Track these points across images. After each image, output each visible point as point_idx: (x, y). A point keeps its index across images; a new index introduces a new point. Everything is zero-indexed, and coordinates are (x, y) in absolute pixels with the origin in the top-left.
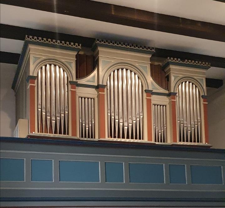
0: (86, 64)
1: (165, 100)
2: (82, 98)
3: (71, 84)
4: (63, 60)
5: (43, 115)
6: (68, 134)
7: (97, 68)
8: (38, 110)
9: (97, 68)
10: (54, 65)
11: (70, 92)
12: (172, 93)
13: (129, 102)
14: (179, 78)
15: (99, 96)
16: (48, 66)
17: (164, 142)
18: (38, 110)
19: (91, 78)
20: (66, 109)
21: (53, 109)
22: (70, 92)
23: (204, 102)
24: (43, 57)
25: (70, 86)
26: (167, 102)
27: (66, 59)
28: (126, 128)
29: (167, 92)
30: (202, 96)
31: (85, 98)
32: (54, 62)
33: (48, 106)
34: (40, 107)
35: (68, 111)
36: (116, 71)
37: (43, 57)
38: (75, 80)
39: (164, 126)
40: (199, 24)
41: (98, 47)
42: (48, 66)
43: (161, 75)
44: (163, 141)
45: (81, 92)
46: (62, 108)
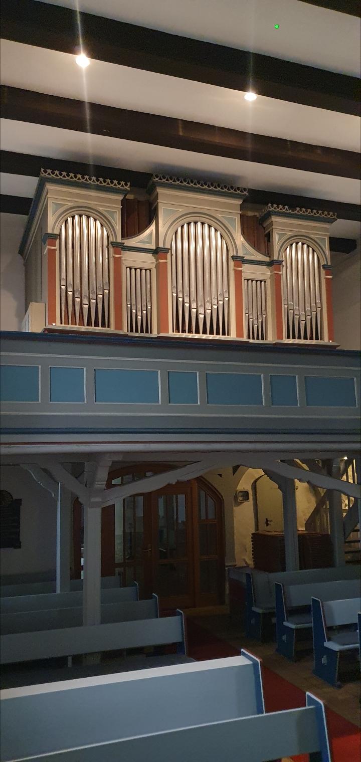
0: (138, 215)
1: (264, 273)
2: (131, 269)
3: (113, 247)
4: (101, 209)
5: (68, 296)
6: (109, 326)
7: (154, 222)
8: (60, 287)
9: (154, 222)
10: (87, 216)
11: (111, 260)
12: (276, 260)
13: (207, 276)
14: (286, 237)
15: (158, 266)
16: (77, 217)
17: (262, 338)
18: (60, 287)
19: (146, 237)
20: (106, 287)
21: (85, 288)
22: (111, 260)
23: (326, 275)
24: (70, 204)
25: (111, 250)
26: (268, 275)
27: (106, 207)
28: (202, 316)
29: (267, 259)
30: (324, 266)
31: (136, 269)
32: (86, 212)
33: (78, 281)
34: (63, 283)
35: (109, 290)
36: (186, 226)
37: (70, 204)
38: (119, 240)
39: (263, 313)
40: (319, 151)
41: (157, 188)
42: (77, 217)
43: (258, 232)
44: (100, 324)
45: (130, 259)
46: (100, 284)
